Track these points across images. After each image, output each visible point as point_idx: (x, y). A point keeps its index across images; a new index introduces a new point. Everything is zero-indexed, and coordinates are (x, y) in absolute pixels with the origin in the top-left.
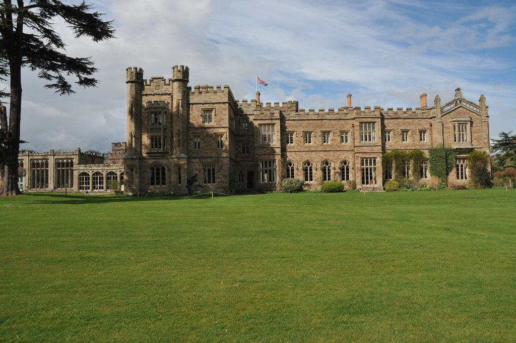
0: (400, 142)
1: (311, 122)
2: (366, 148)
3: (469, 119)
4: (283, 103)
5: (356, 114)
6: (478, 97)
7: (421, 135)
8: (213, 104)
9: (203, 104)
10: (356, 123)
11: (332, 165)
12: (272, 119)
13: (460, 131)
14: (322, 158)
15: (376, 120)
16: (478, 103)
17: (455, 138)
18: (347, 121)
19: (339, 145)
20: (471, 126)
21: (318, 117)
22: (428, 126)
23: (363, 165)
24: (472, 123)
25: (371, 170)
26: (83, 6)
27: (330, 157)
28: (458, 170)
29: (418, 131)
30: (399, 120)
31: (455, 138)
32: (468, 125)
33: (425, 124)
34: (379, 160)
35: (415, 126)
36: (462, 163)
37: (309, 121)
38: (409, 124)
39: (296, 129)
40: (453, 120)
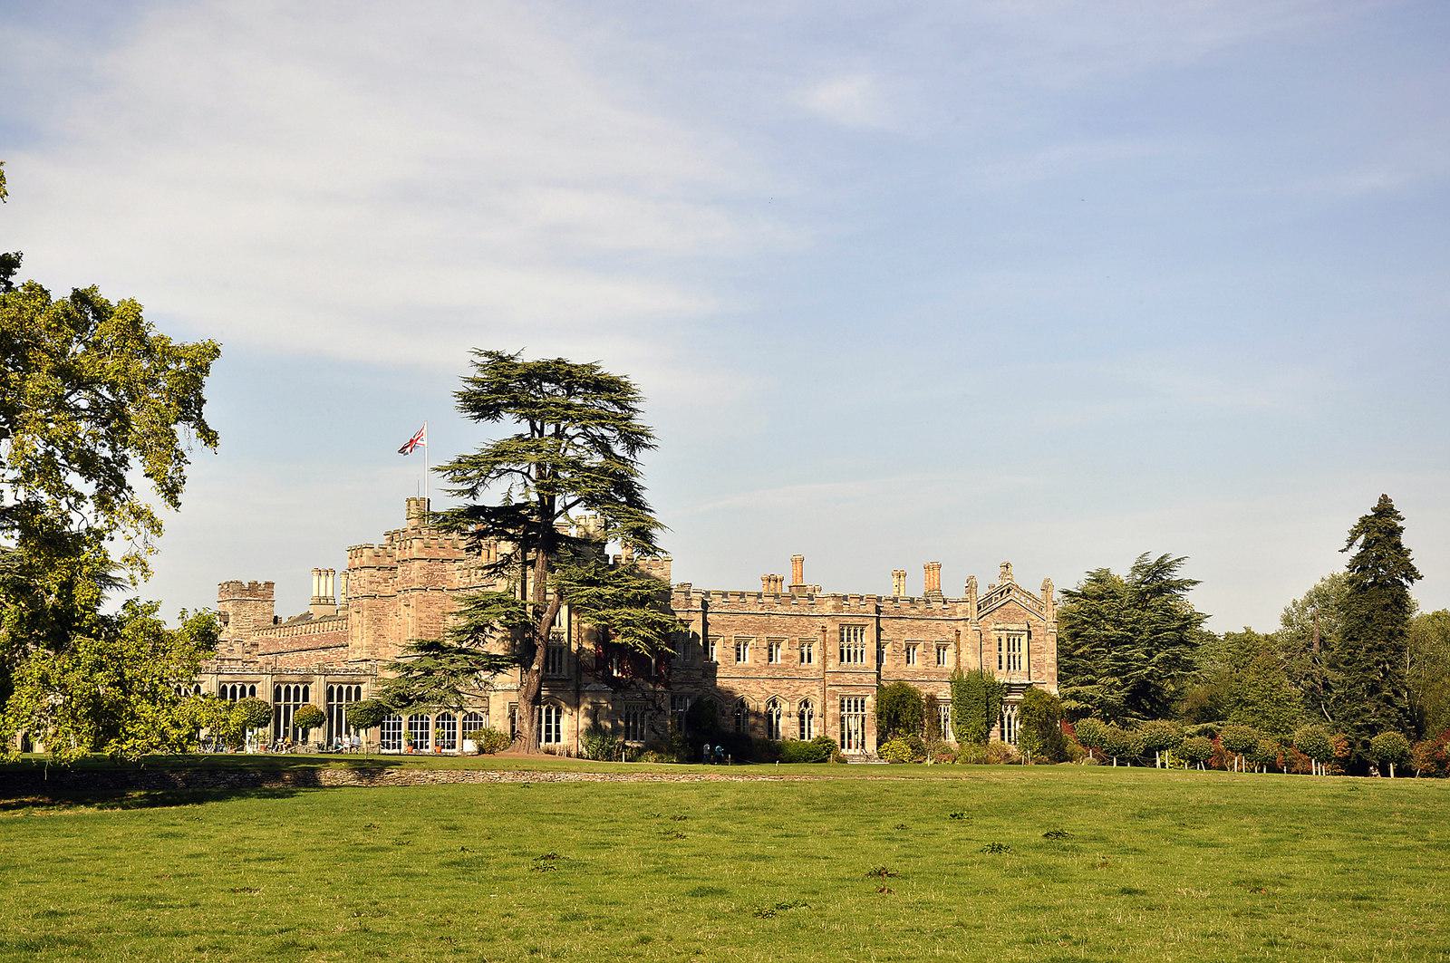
0: (903, 666)
2: (849, 676)
3: (1026, 627)
5: (834, 607)
6: (1040, 586)
7: (939, 653)
10: (833, 627)
11: (785, 707)
13: (1009, 650)
15: (868, 621)
16: (1039, 595)
17: (1000, 662)
18: (812, 619)
19: (798, 667)
20: (1029, 637)
21: (761, 609)
22: (952, 636)
23: (844, 710)
24: (1029, 633)
26: (94, 288)
28: (1002, 726)
29: (934, 644)
30: (903, 621)
31: (1000, 662)
32: (1024, 639)
34: (870, 700)
36: (1009, 711)
37: (745, 616)
38: (920, 630)
39: (722, 632)
40: (998, 627)
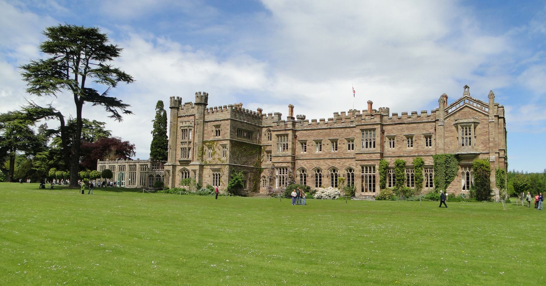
1: (321, 131)
4: (363, 111)
8: (221, 121)
9: (214, 121)
12: (286, 130)
14: (329, 165)
15: (376, 127)
16: (486, 101)
22: (432, 131)
25: (283, 178)
27: (336, 164)
33: (429, 128)
35: (418, 131)
38: (413, 129)
